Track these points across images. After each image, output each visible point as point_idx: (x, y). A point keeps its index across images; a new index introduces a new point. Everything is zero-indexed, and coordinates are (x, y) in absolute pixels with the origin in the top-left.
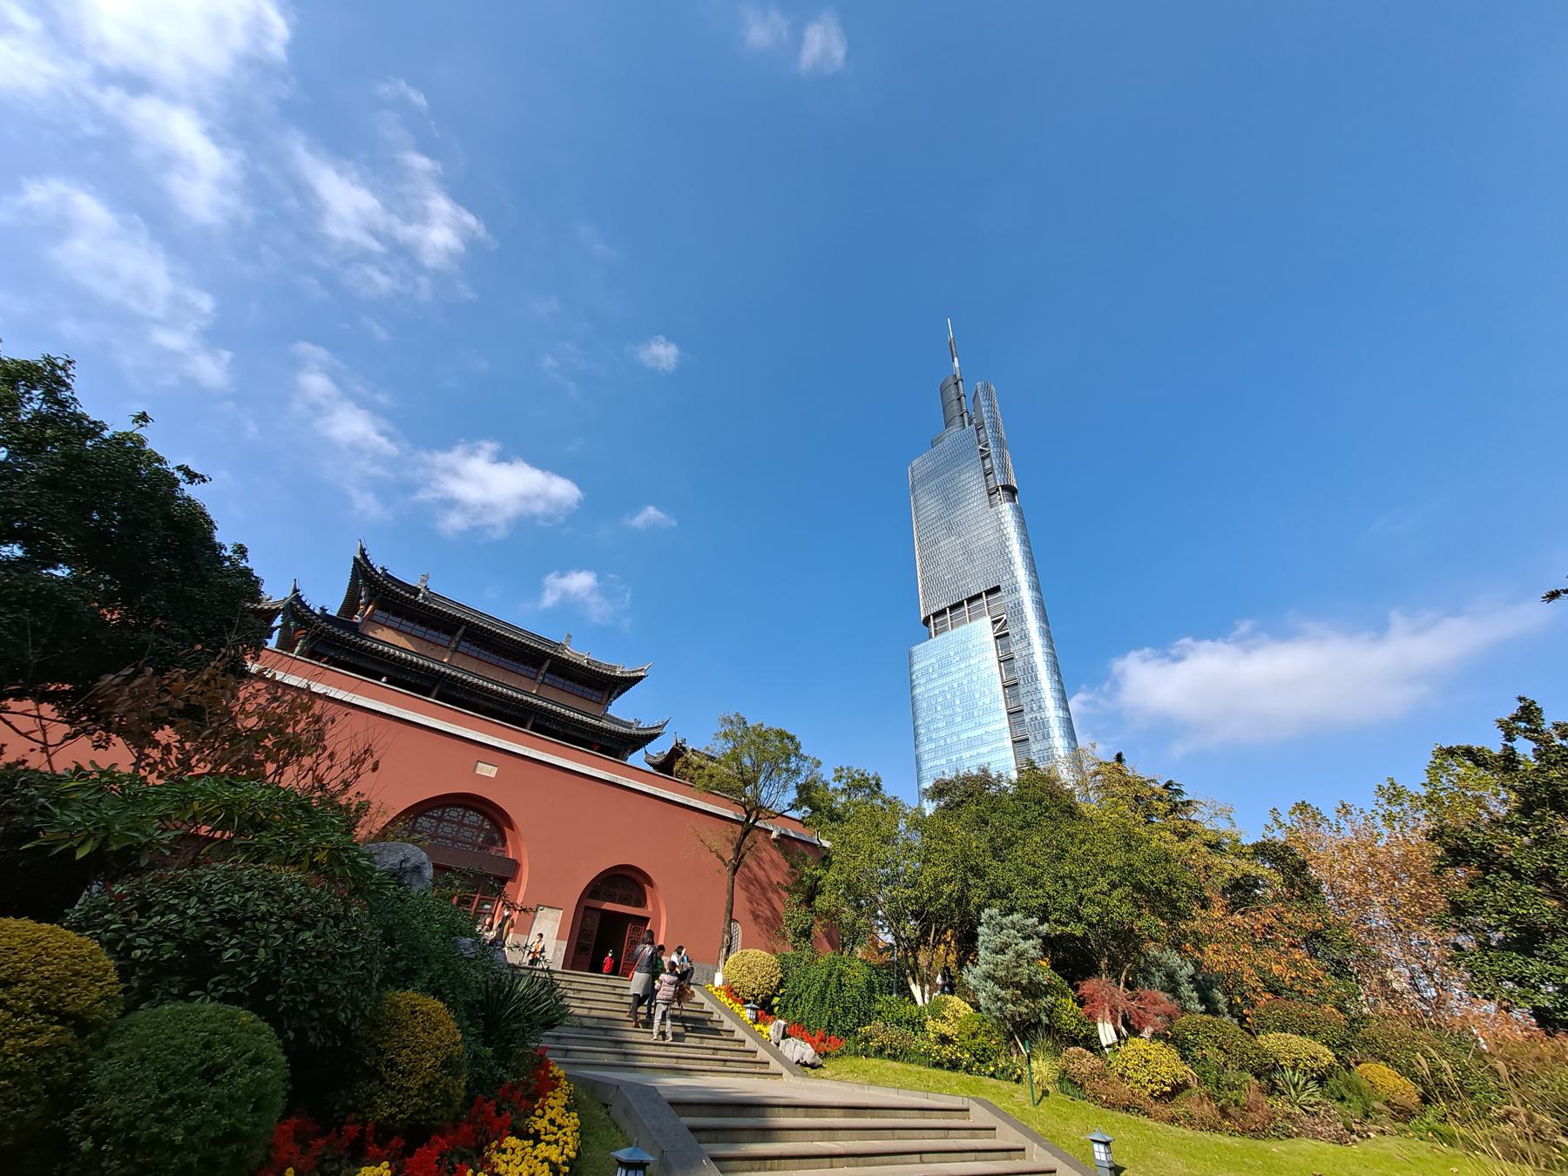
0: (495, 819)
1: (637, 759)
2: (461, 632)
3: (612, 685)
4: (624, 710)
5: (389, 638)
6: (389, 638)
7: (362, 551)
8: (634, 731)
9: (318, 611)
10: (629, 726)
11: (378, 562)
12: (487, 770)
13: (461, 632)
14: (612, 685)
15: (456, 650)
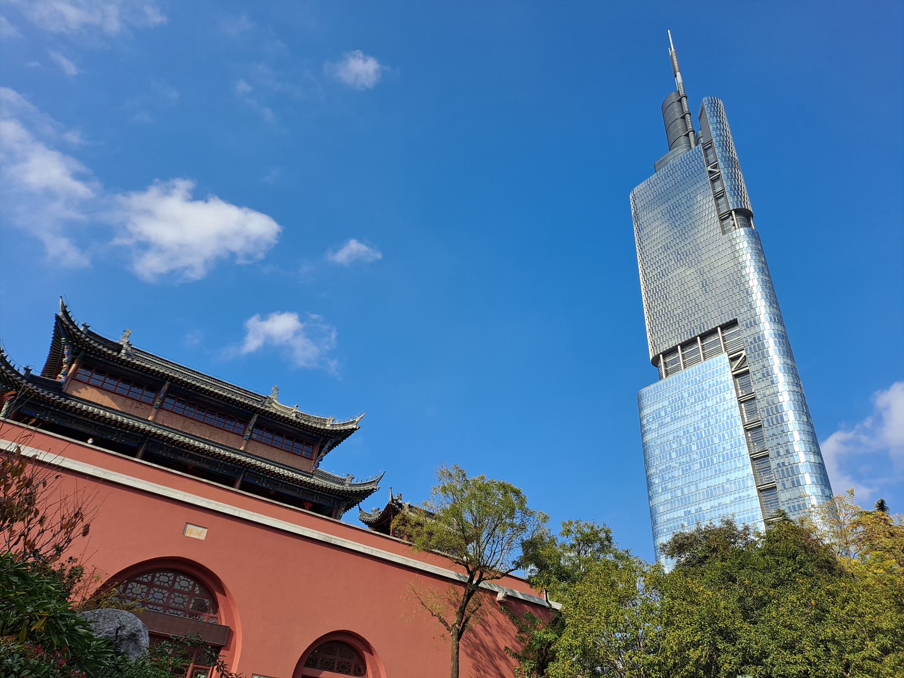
0: (205, 583)
1: (351, 517)
2: (165, 387)
3: (320, 440)
4: (336, 467)
5: (93, 397)
6: (93, 397)
7: (64, 308)
8: (347, 487)
9: (22, 372)
10: (342, 482)
11: (80, 319)
12: (196, 533)
13: (165, 387)
14: (320, 440)
15: (160, 408)
